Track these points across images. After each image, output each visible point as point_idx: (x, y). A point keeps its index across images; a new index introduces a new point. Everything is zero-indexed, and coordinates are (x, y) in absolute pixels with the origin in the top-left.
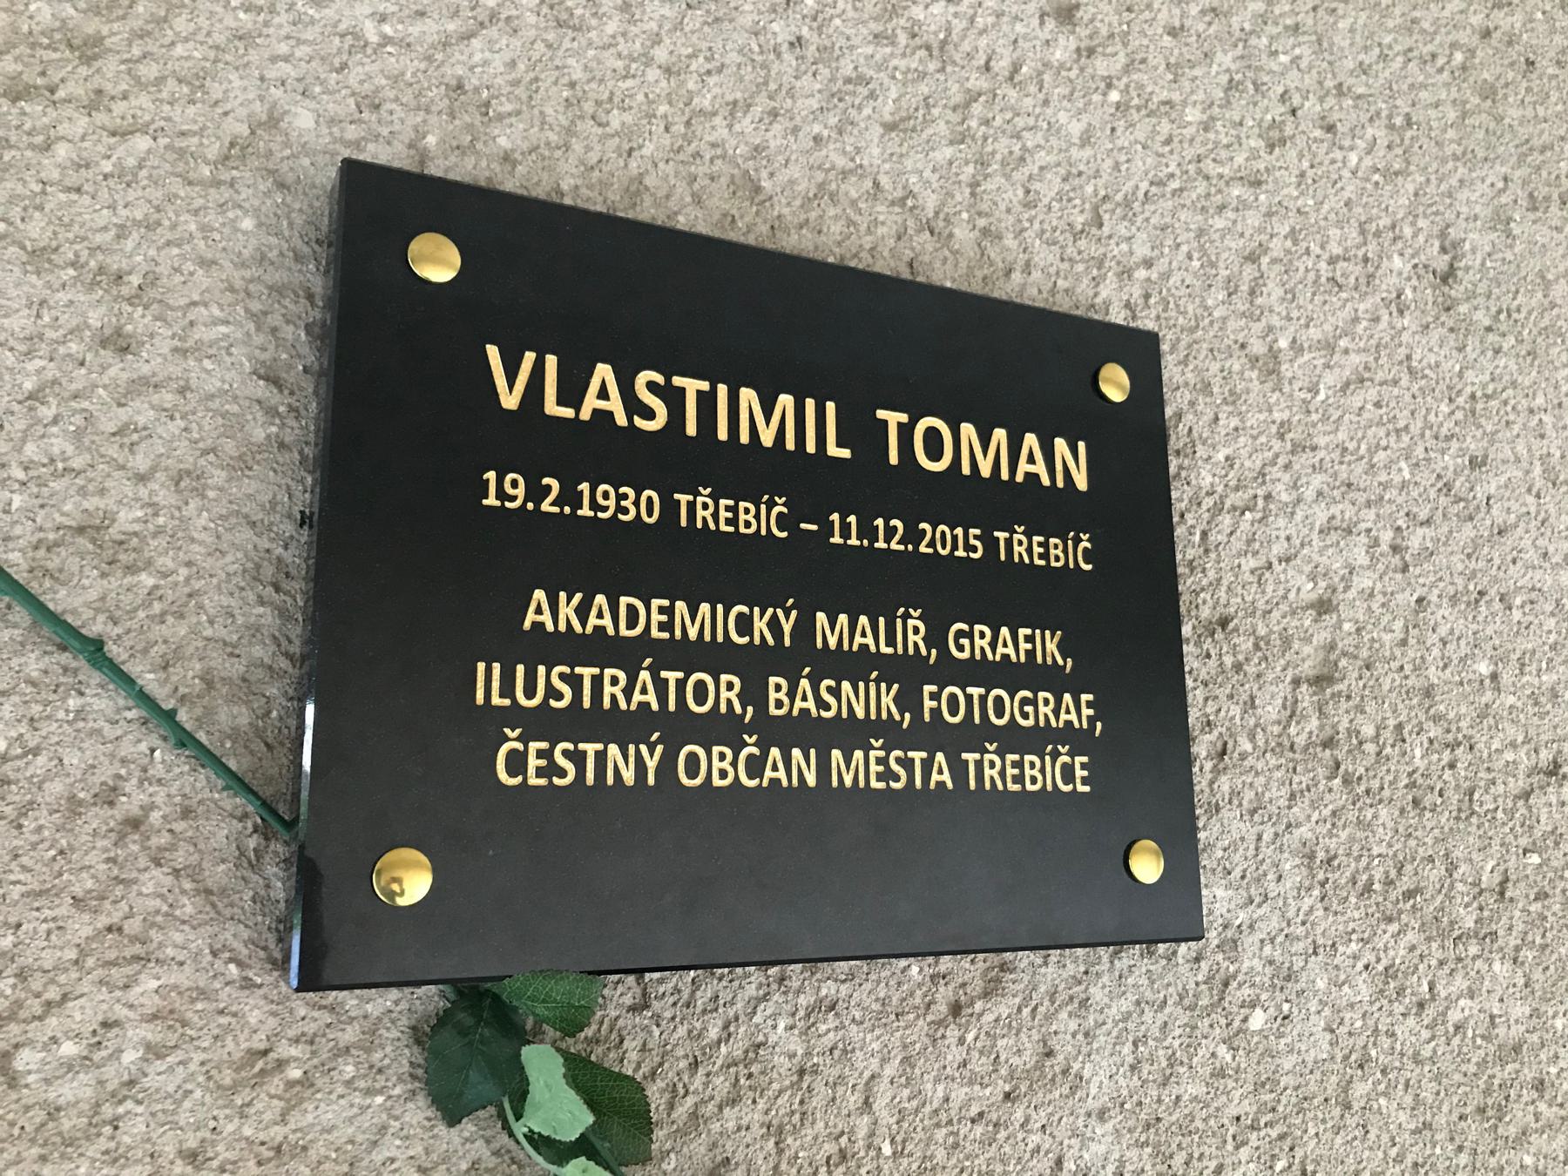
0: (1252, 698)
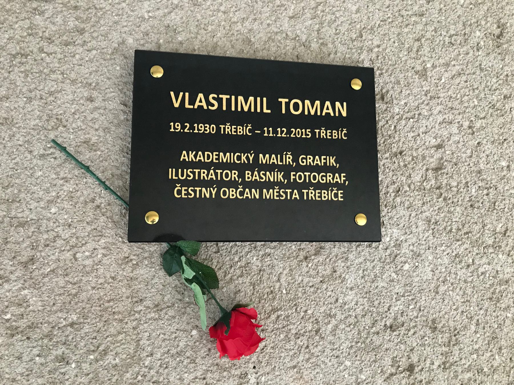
0: (410, 175)
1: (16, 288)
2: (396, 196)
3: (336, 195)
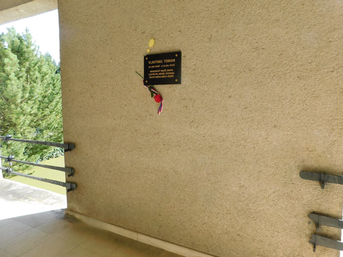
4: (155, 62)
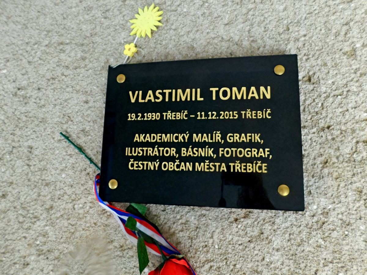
0: (339, 147)
1: (43, 225)
2: (323, 167)
3: (260, 168)
4: (163, 94)
